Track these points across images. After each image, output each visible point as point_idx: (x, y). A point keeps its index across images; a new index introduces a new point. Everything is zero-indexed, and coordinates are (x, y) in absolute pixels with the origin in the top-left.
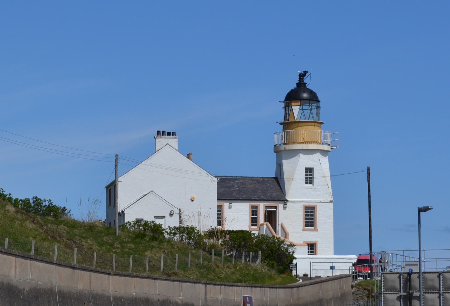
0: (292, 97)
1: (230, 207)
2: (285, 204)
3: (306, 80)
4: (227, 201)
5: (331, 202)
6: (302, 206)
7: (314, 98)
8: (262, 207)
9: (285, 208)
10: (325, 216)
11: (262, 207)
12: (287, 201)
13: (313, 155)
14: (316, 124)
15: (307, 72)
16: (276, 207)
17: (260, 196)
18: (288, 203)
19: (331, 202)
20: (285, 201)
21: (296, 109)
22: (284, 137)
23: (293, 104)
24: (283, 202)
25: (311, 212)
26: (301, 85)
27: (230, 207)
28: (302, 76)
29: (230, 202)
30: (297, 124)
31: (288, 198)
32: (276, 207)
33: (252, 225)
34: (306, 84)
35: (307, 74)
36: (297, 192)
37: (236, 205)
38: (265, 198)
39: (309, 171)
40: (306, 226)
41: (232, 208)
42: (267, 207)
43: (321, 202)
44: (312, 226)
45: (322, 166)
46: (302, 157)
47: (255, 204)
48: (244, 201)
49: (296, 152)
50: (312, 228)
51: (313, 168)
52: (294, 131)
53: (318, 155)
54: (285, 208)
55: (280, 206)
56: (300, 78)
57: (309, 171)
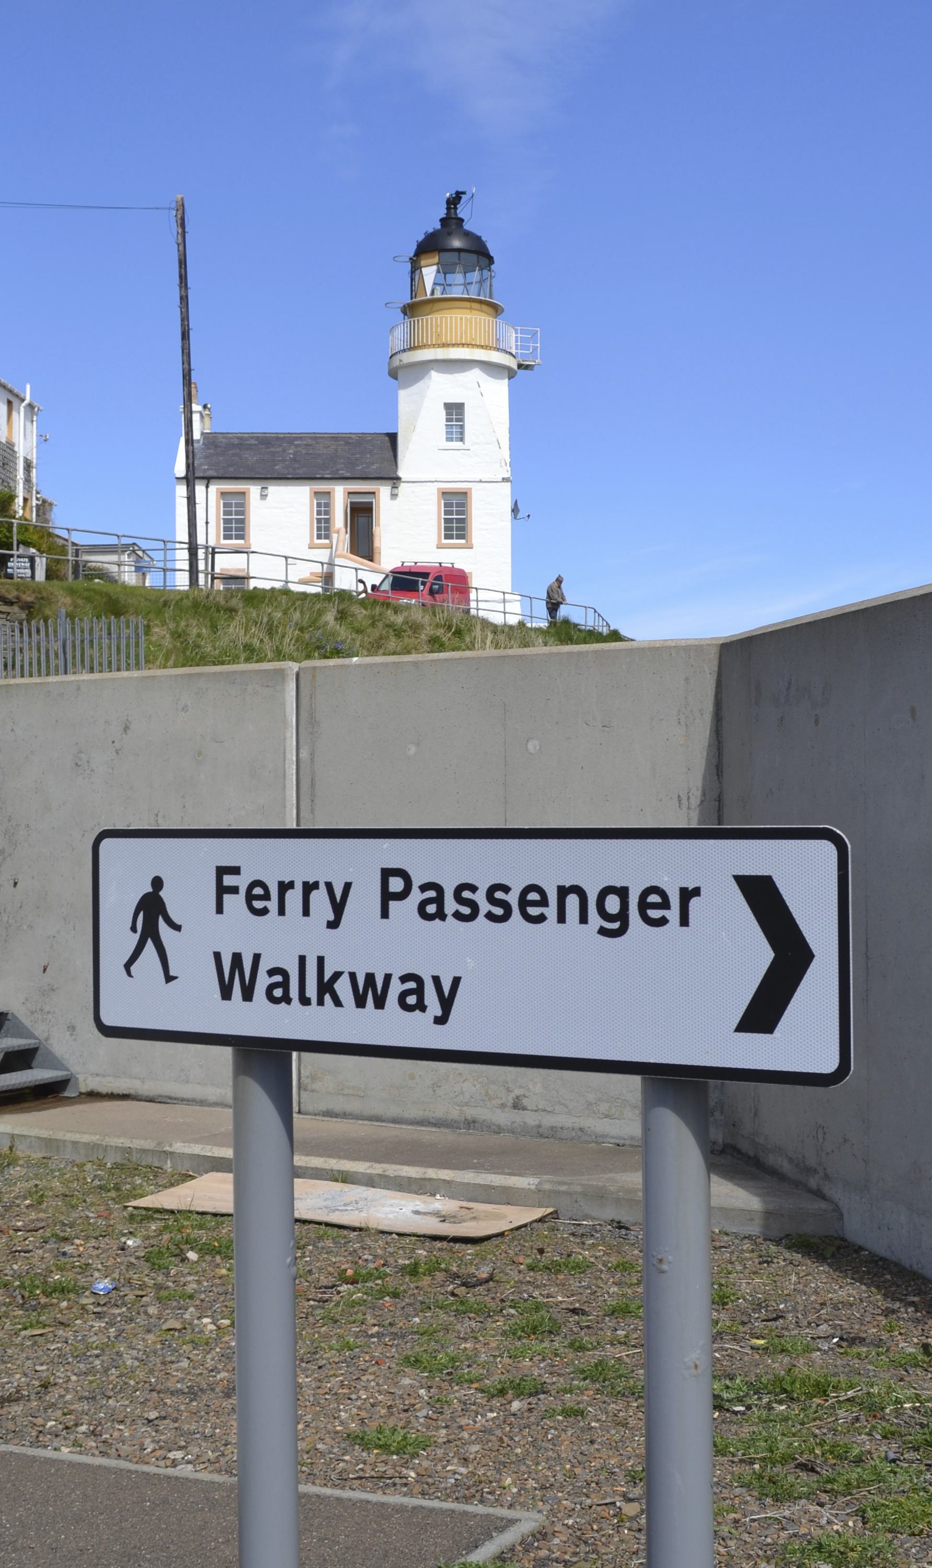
0: (429, 246)
1: (263, 497)
2: (395, 487)
3: (462, 211)
4: (256, 481)
5: (505, 480)
6: (436, 492)
7: (479, 253)
8: (340, 494)
9: (394, 496)
10: (491, 514)
11: (340, 494)
12: (399, 479)
13: (463, 374)
14: (475, 305)
15: (464, 193)
16: (243, 494)
17: (338, 470)
18: (403, 487)
19: (505, 480)
20: (394, 480)
21: (429, 273)
22: (412, 332)
23: (423, 263)
24: (391, 482)
25: (458, 505)
26: (451, 222)
27: (263, 497)
28: (454, 201)
29: (264, 483)
30: (429, 306)
31: (401, 473)
32: (243, 494)
33: (319, 537)
34: (462, 220)
35: (464, 198)
36: (425, 458)
37: (279, 492)
38: (348, 475)
39: (455, 411)
40: (447, 537)
41: (398, 499)
42: (223, 494)
43: (481, 481)
44: (459, 537)
45: (489, 400)
46: (435, 377)
47: (323, 487)
48: (222, 481)
49: (425, 367)
50: (463, 541)
51: (445, 404)
52: (427, 320)
53: (476, 374)
54: (394, 496)
55: (384, 491)
56: (448, 209)
57: (455, 411)
